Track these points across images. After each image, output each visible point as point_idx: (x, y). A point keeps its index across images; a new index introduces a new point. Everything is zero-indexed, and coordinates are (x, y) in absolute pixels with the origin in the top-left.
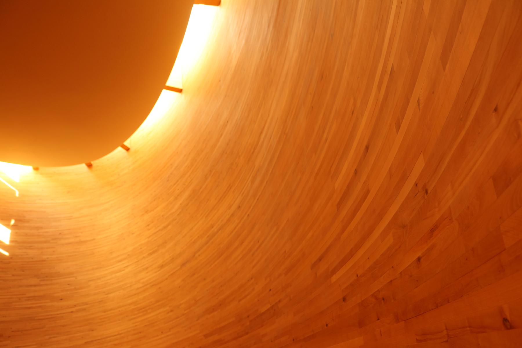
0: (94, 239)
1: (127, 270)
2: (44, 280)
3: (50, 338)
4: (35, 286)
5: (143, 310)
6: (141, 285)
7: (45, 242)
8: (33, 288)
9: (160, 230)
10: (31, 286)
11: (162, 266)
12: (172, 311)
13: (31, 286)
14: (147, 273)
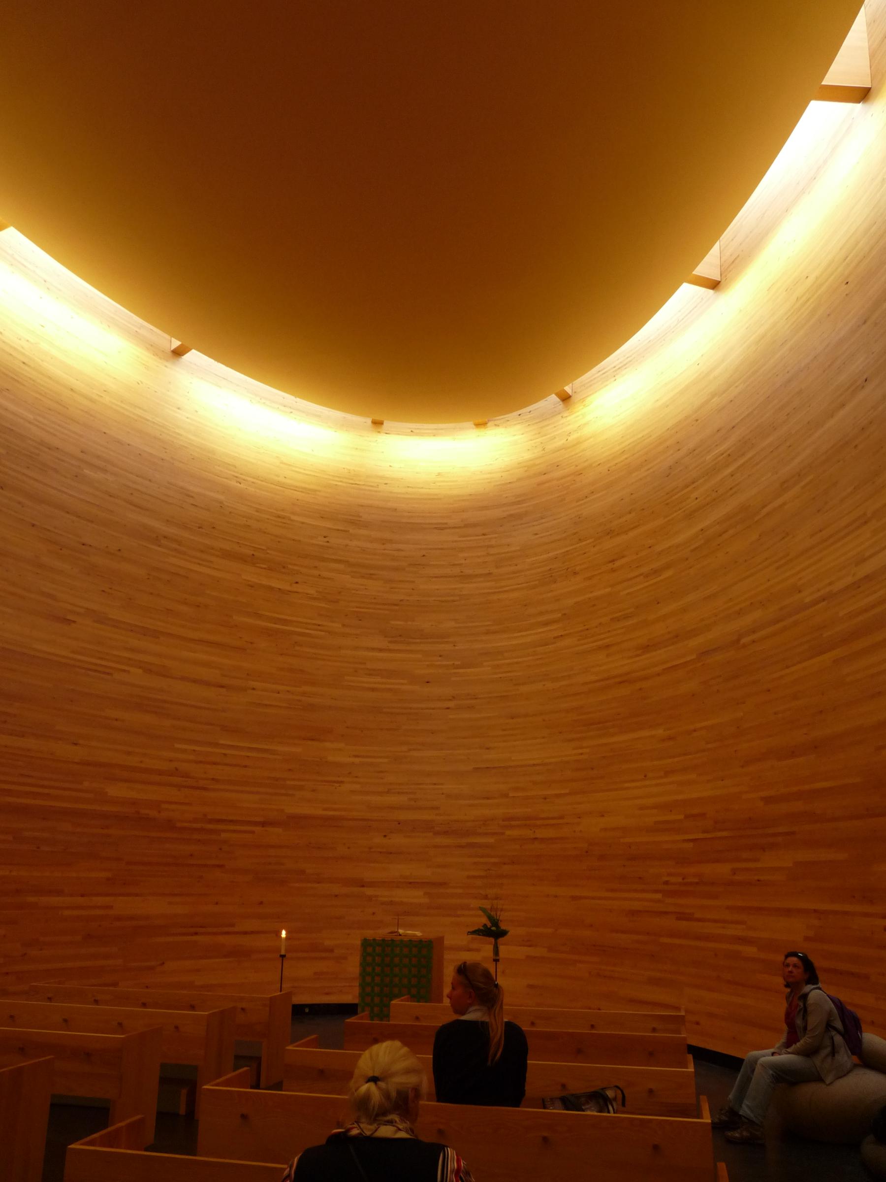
6: (593, 678)
11: (646, 648)
14: (608, 656)
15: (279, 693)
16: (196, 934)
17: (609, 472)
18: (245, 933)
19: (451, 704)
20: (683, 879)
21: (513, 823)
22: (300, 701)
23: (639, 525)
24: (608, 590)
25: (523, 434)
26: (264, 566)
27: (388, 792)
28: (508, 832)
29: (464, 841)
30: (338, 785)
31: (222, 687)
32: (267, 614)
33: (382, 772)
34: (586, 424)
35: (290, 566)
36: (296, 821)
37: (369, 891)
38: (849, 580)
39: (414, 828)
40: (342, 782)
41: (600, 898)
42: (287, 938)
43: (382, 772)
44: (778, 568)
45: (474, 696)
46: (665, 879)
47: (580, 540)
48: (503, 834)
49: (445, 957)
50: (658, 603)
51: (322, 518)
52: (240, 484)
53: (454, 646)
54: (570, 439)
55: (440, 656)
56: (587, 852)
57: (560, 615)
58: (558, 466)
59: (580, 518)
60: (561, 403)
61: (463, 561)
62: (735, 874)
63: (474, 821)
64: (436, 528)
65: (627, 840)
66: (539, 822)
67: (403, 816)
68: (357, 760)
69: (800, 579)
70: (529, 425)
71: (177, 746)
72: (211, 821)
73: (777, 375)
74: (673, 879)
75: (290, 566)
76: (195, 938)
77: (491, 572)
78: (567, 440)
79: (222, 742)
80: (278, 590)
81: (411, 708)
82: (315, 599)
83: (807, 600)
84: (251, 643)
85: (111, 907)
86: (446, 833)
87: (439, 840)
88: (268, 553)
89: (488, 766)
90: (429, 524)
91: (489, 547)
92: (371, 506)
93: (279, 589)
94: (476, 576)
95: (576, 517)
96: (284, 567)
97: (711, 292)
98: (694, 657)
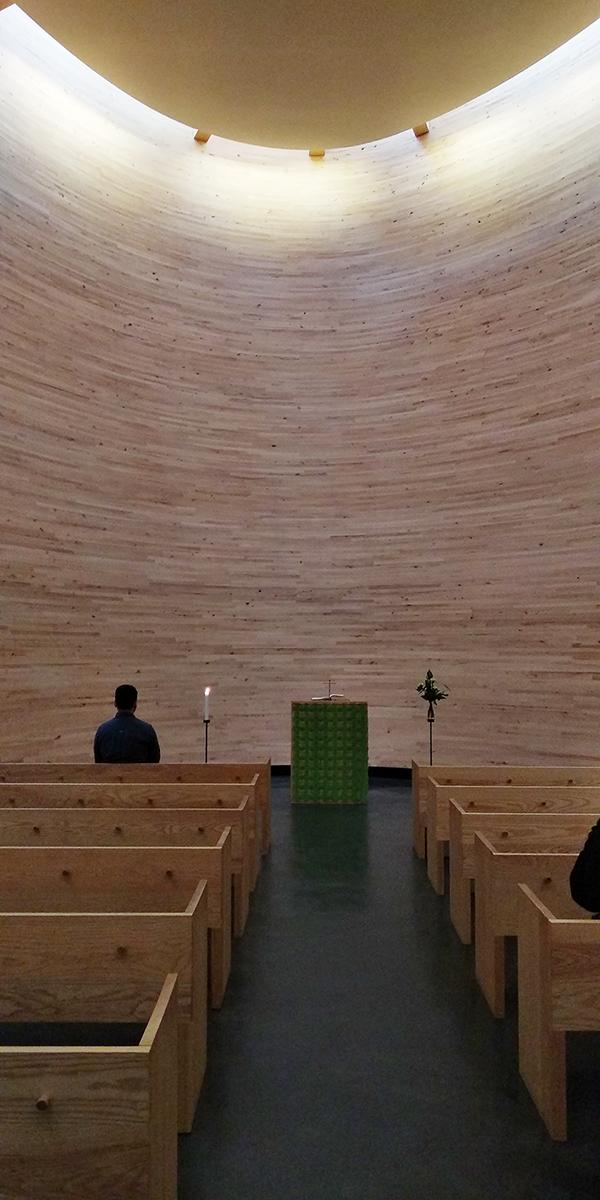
1: (423, 410)
2: (236, 400)
3: (261, 517)
5: (477, 495)
7: (231, 318)
8: (216, 413)
9: (526, 339)
10: (216, 407)
12: (572, 508)
13: (216, 407)
21: (382, 591)
22: (147, 460)
23: (522, 285)
24: (482, 354)
26: (95, 301)
28: (375, 599)
30: (193, 551)
33: (235, 539)
36: (160, 588)
37: (237, 658)
40: (198, 549)
43: (235, 539)
46: (575, 642)
48: (372, 601)
49: (114, 699)
57: (420, 380)
60: (416, 139)
66: (410, 590)
67: (265, 583)
75: (124, 306)
81: (258, 473)
82: (147, 344)
88: (98, 286)
92: (198, 241)
95: (435, 273)
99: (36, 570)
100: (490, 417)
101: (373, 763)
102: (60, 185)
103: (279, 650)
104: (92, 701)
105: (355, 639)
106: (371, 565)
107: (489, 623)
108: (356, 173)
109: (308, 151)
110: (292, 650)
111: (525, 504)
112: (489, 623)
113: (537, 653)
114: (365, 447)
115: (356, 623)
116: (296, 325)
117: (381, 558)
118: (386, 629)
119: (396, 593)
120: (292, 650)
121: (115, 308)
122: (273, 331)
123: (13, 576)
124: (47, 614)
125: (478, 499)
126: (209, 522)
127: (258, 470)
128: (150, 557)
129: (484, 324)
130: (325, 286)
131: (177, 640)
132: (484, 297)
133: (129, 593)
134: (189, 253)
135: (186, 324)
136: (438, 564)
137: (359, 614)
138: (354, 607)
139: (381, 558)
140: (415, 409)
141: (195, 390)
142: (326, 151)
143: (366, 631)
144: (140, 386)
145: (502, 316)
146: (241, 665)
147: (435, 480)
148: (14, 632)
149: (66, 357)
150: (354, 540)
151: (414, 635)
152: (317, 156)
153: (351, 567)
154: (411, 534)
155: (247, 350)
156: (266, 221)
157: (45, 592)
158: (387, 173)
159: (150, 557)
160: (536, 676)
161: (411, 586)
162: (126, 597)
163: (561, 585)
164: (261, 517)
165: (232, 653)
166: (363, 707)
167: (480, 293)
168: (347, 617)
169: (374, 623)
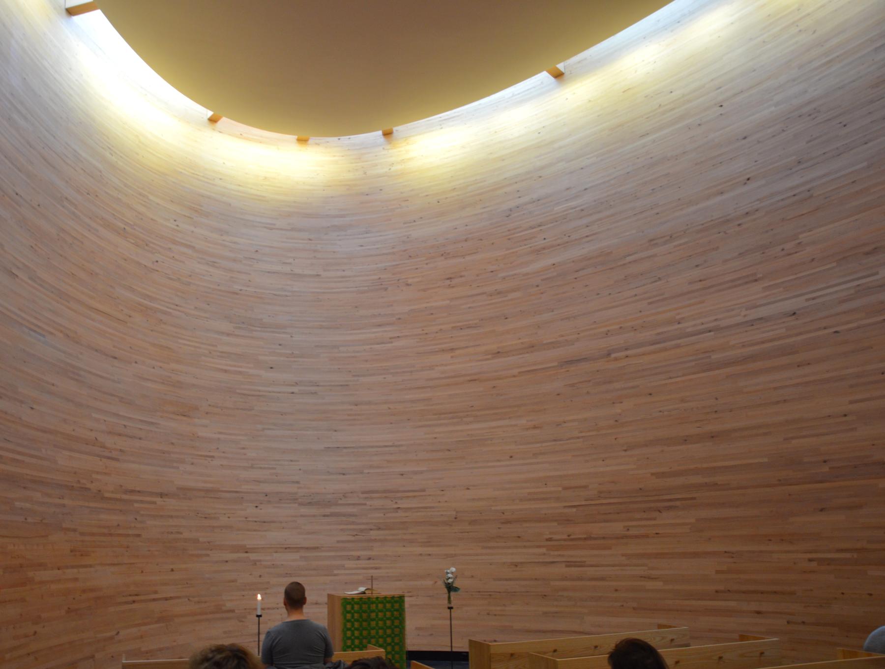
0: (318, 275)
2: (240, 328)
3: (263, 429)
4: (228, 335)
5: (451, 415)
7: (235, 260)
8: (225, 338)
11: (498, 354)
12: (535, 427)
13: (222, 333)
14: (452, 357)
15: (154, 368)
16: (134, 602)
17: (438, 204)
18: (166, 599)
19: (295, 389)
20: (569, 536)
23: (477, 252)
25: (343, 156)
26: (133, 242)
27: (252, 467)
29: (328, 511)
30: (210, 459)
31: (115, 358)
32: (140, 289)
33: (243, 448)
34: (410, 159)
35: (151, 245)
36: (185, 492)
37: (253, 556)
38: (739, 319)
39: (280, 500)
40: (213, 457)
41: (477, 555)
42: (262, 599)
43: (243, 448)
44: (650, 303)
45: (316, 383)
47: (410, 256)
48: (365, 504)
50: (506, 318)
51: (172, 201)
52: (112, 155)
53: (292, 337)
54: (393, 169)
55: (280, 345)
56: (456, 518)
58: (381, 190)
59: (408, 238)
60: (382, 137)
61: (291, 260)
62: (628, 530)
63: (333, 494)
64: (265, 227)
65: (498, 508)
66: (399, 495)
68: (222, 436)
69: (679, 314)
70: (349, 150)
71: (94, 415)
72: (126, 492)
73: (638, 158)
74: (555, 537)
75: (151, 245)
76: (134, 606)
77: (319, 273)
78: (390, 169)
79: (121, 413)
80: (144, 266)
81: (259, 391)
82: (171, 279)
83: (689, 330)
84: (130, 316)
85: (76, 580)
86: (310, 504)
87: (304, 510)
88: (135, 229)
89: (339, 446)
90: (259, 222)
91: (315, 251)
92: (209, 197)
93: (145, 266)
94: (305, 276)
96: (147, 245)
97: (552, 79)
98: (555, 364)
99: (95, 476)
100: (458, 352)
101: (410, 648)
102: (110, 147)
103: (286, 548)
104: (142, 598)
105: (353, 538)
106: (362, 473)
107: (472, 522)
108: (334, 156)
109: (296, 137)
110: (298, 549)
111: (494, 424)
112: (472, 522)
113: (516, 547)
114: (350, 371)
115: (353, 523)
116: (287, 269)
117: (371, 467)
118: (379, 529)
119: (386, 497)
120: (298, 549)
121: (146, 247)
122: (269, 272)
123: (79, 482)
124: (103, 516)
125: (453, 418)
126: (221, 433)
127: (260, 388)
128: (175, 465)
129: (448, 279)
130: (310, 240)
131: (201, 539)
132: (446, 258)
133: (161, 497)
134: (202, 206)
135: (199, 263)
136: (421, 472)
137: (356, 516)
138: (350, 510)
139: (371, 467)
140: (392, 342)
141: (207, 318)
142: (311, 138)
143: (362, 531)
144: (165, 313)
145: (463, 274)
146: (255, 563)
147: (413, 401)
148: (82, 534)
149: (111, 286)
150: (345, 450)
151: (405, 534)
152: (302, 141)
153: (344, 474)
154: (396, 446)
155: (248, 286)
156: (262, 186)
157: (99, 496)
158: (360, 158)
159: (175, 465)
160: (516, 566)
161: (398, 492)
162: (158, 500)
163: (533, 490)
164: (263, 429)
165: (247, 552)
166: (401, 598)
167: (442, 255)
168: (344, 519)
169: (367, 524)
